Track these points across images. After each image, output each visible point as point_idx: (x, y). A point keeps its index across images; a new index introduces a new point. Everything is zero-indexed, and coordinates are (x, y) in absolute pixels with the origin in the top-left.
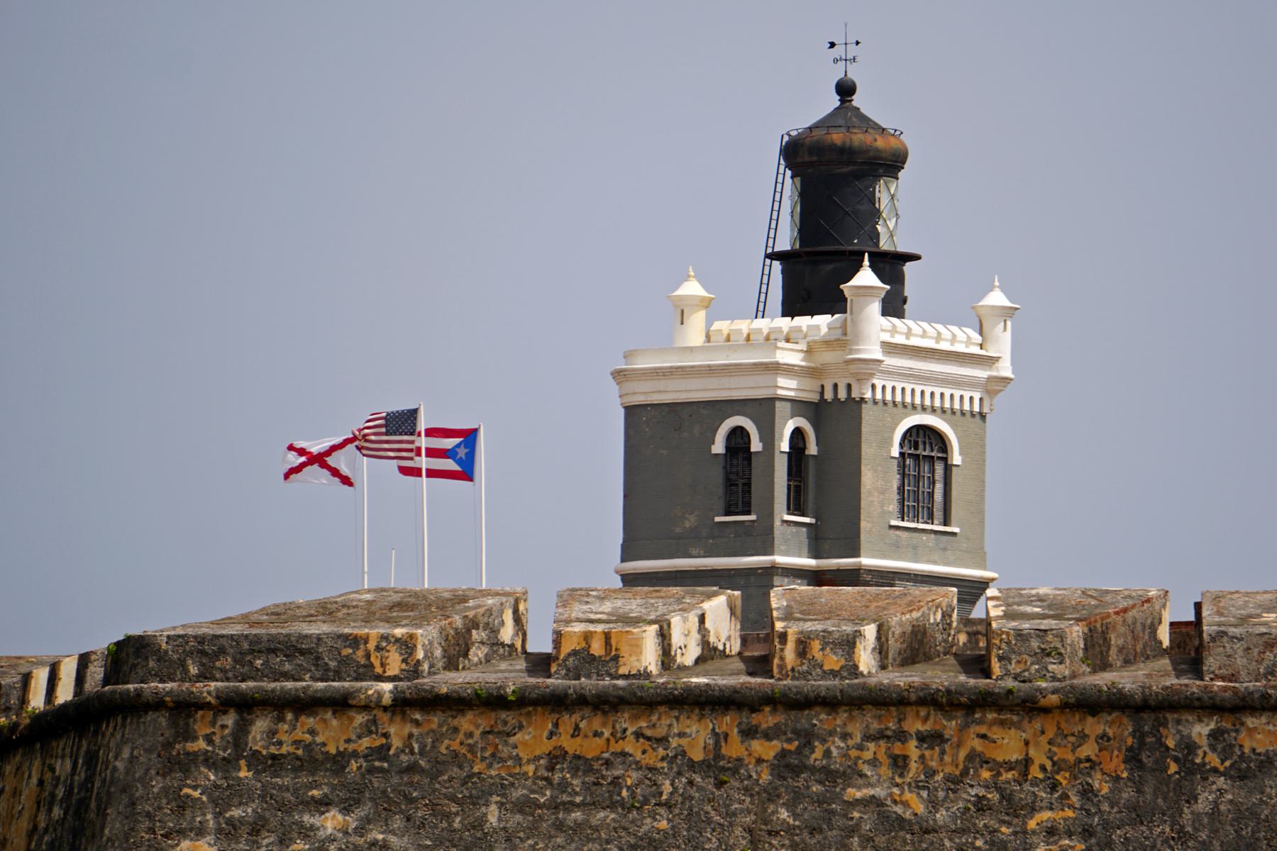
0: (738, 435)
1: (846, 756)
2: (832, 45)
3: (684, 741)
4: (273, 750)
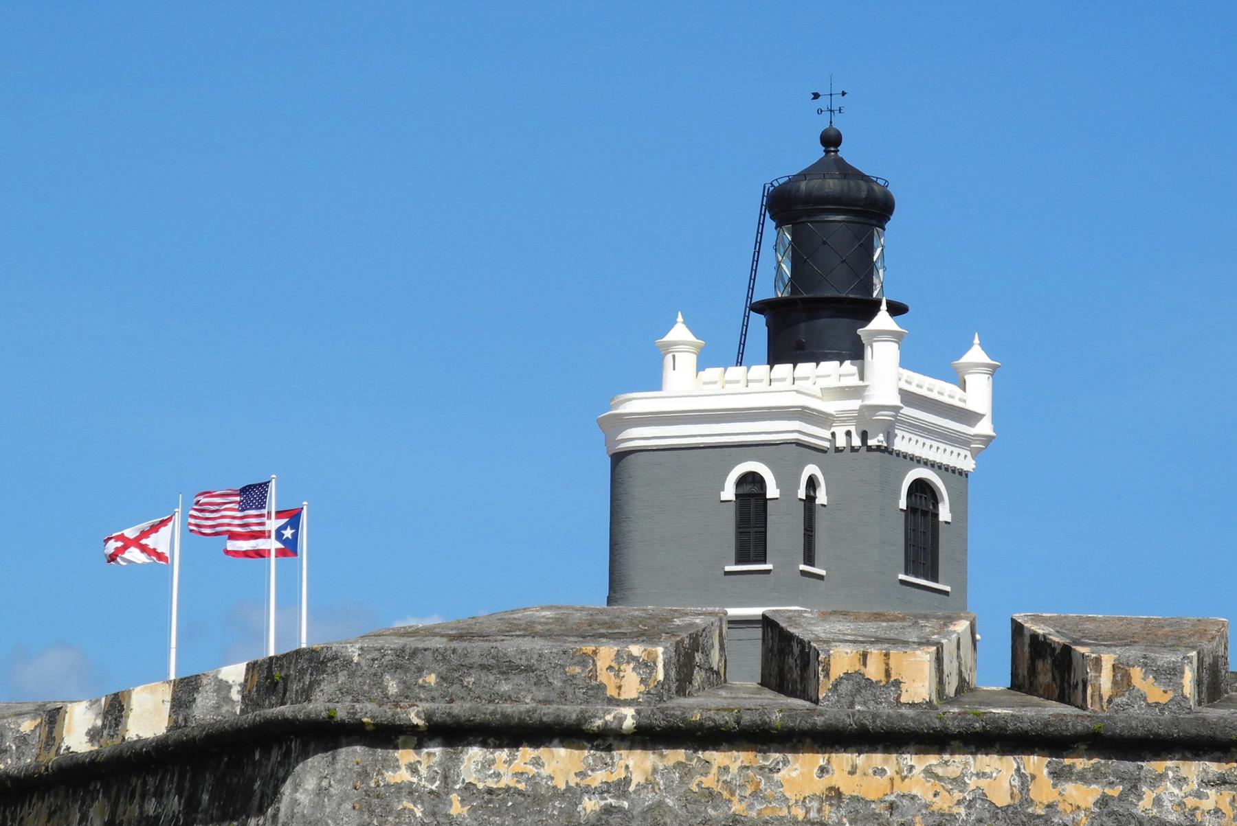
0: (751, 482)
1: (1181, 804)
2: (816, 96)
3: (983, 783)
4: (491, 783)
